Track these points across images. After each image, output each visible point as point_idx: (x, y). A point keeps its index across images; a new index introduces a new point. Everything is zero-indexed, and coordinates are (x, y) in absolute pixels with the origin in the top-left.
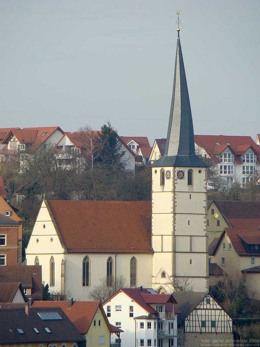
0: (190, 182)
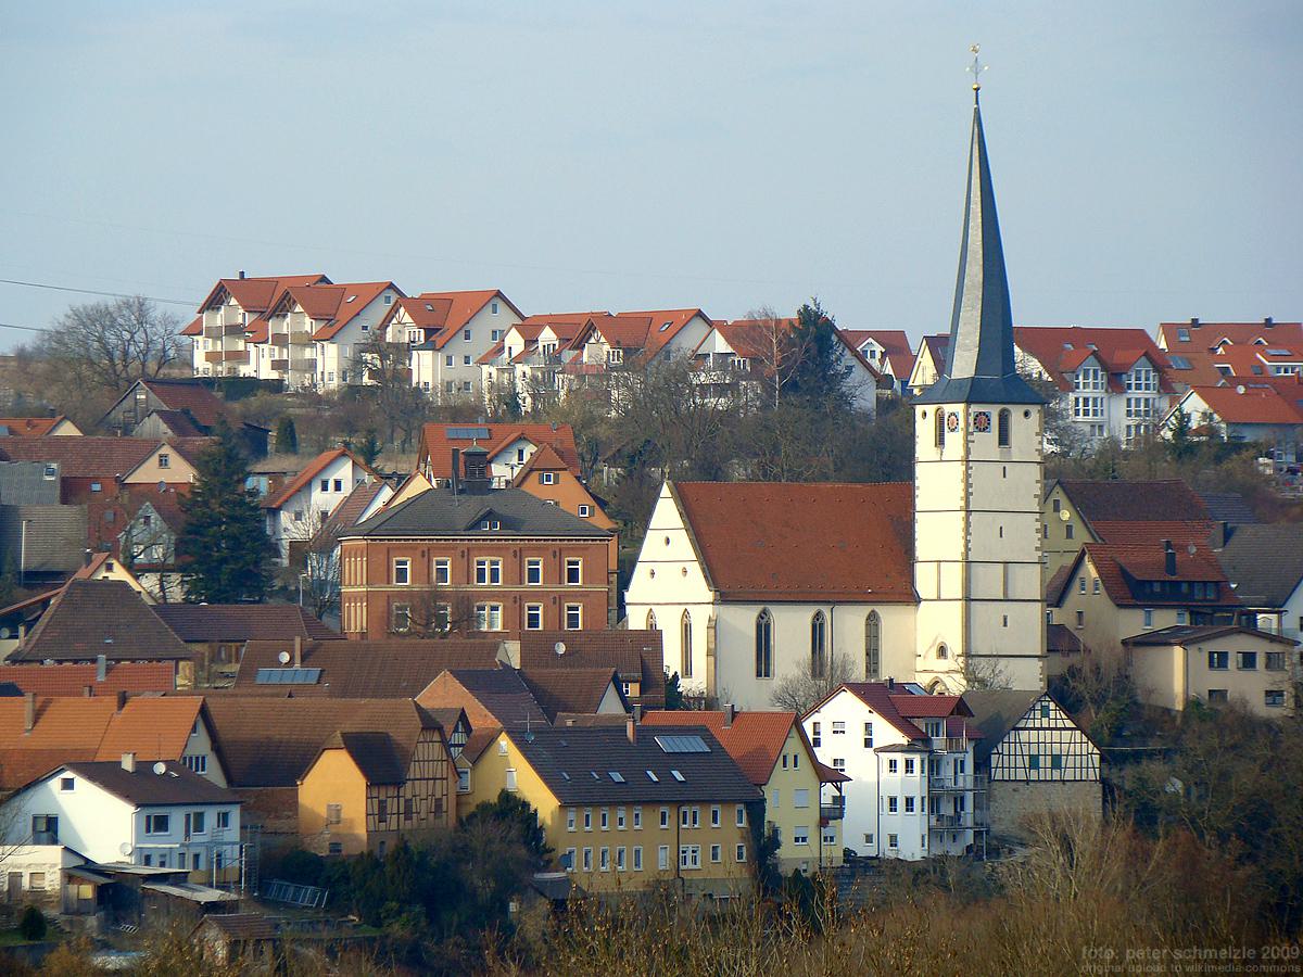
0: (1004, 439)
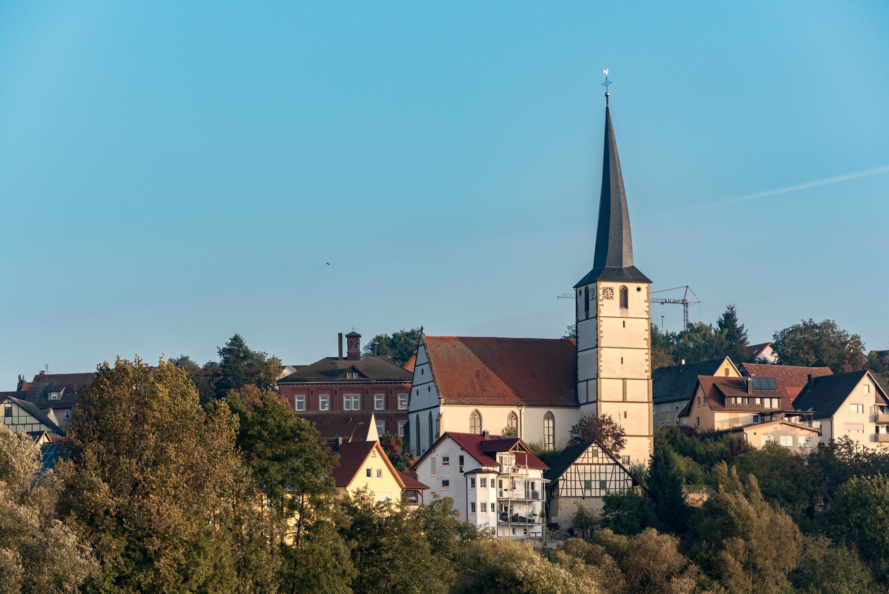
0: (624, 304)
